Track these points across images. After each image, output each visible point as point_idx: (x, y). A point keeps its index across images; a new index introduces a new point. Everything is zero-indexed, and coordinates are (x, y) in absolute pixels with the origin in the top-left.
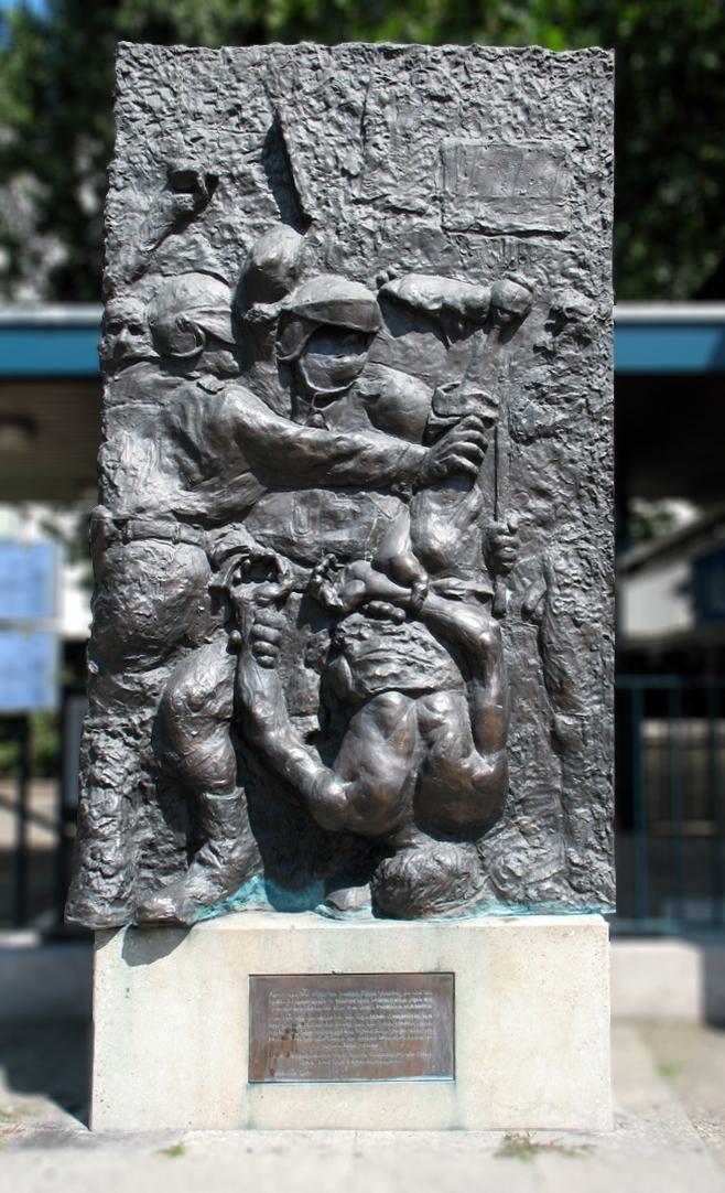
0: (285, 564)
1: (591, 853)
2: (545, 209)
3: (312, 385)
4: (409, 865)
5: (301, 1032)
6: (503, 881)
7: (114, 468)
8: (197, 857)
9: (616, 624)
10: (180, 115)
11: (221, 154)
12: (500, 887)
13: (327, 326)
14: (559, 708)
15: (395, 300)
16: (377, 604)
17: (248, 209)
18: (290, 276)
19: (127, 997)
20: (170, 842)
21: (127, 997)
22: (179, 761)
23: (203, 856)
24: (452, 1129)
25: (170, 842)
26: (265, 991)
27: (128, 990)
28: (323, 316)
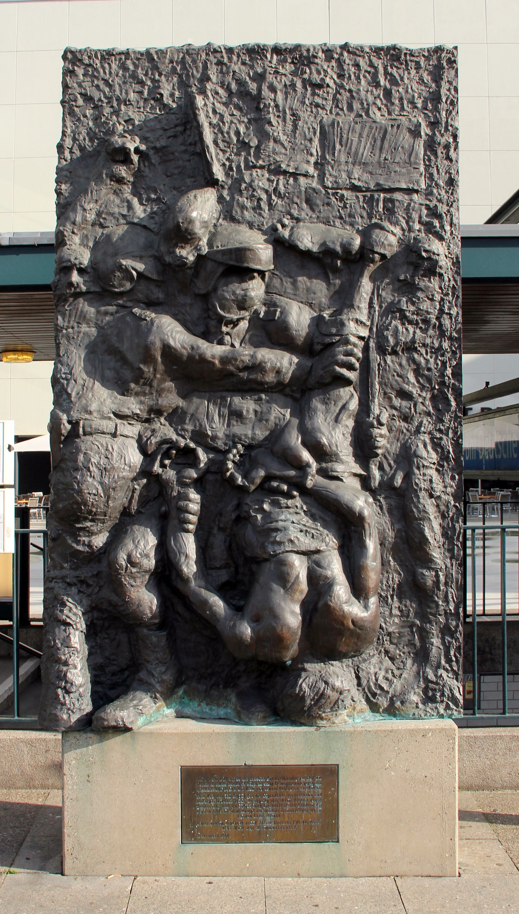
0: (203, 456)
1: (441, 671)
2: (404, 170)
3: (222, 313)
4: (304, 685)
5: (213, 805)
6: (374, 695)
7: (66, 379)
8: (137, 677)
9: (457, 445)
10: (321, 539)
11: (147, 132)
12: (372, 699)
13: (233, 266)
14: (418, 562)
15: (287, 245)
16: (275, 484)
17: (169, 174)
18: (204, 227)
19: (88, 781)
20: (115, 665)
21: (88, 781)
22: (122, 606)
23: (142, 677)
24: (210, 883)
25: (115, 665)
26: (194, 779)
27: (88, 776)
28: (231, 259)
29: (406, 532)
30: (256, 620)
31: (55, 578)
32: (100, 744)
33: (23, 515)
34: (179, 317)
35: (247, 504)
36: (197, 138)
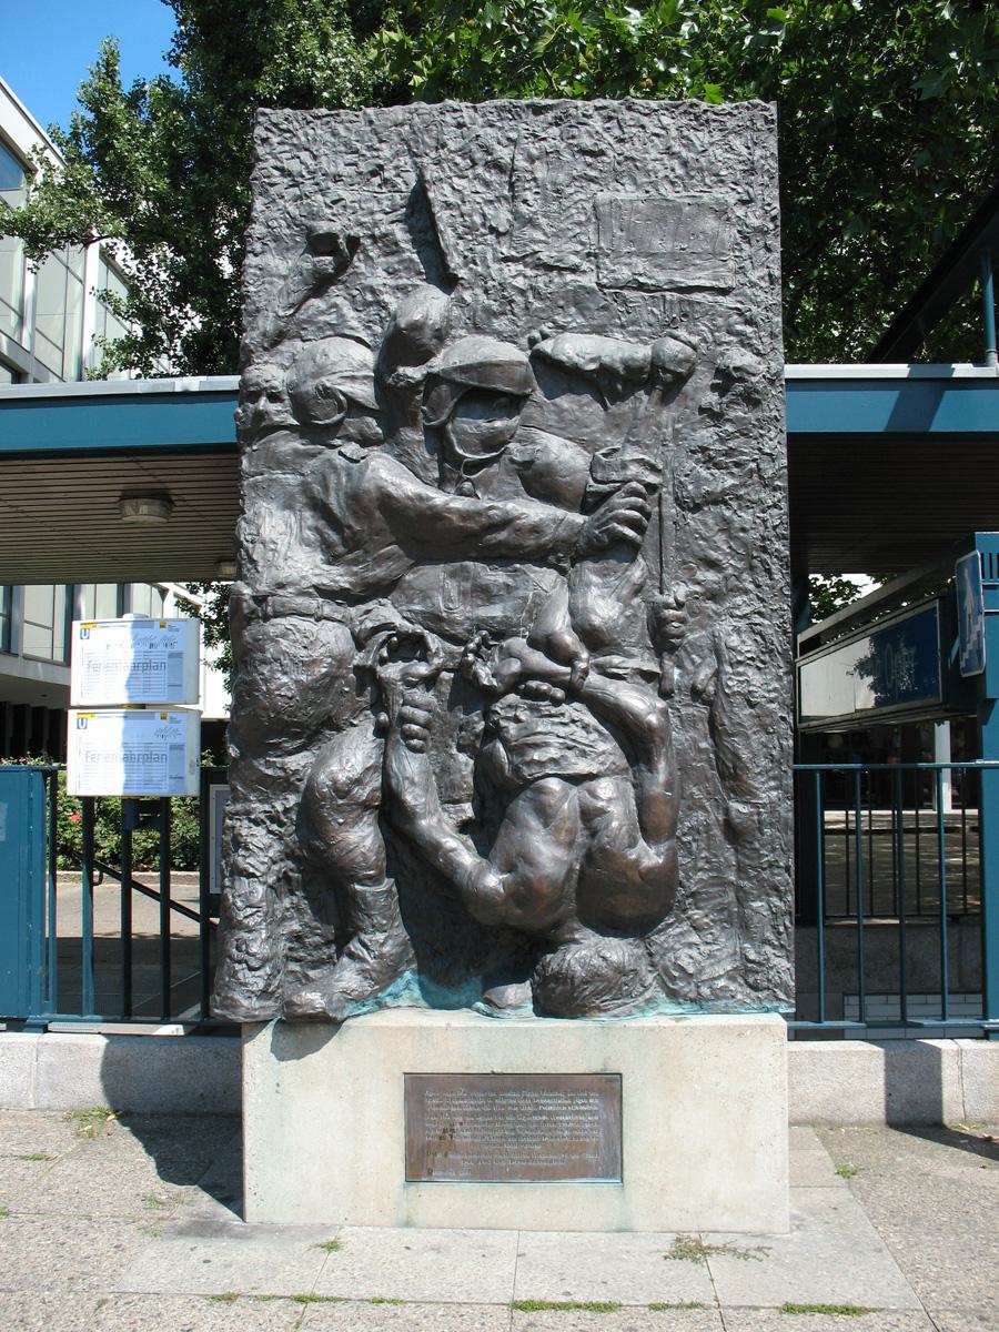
3: (461, 452)
5: (453, 1130)
6: (673, 979)
8: (346, 950)
13: (475, 388)
16: (533, 684)
26: (419, 1088)
29: (715, 753)
30: (510, 868)
31: (237, 813)
32: (120, 753)
33: (478, 1010)
34: (404, 459)
35: (496, 712)
36: (428, 223)
